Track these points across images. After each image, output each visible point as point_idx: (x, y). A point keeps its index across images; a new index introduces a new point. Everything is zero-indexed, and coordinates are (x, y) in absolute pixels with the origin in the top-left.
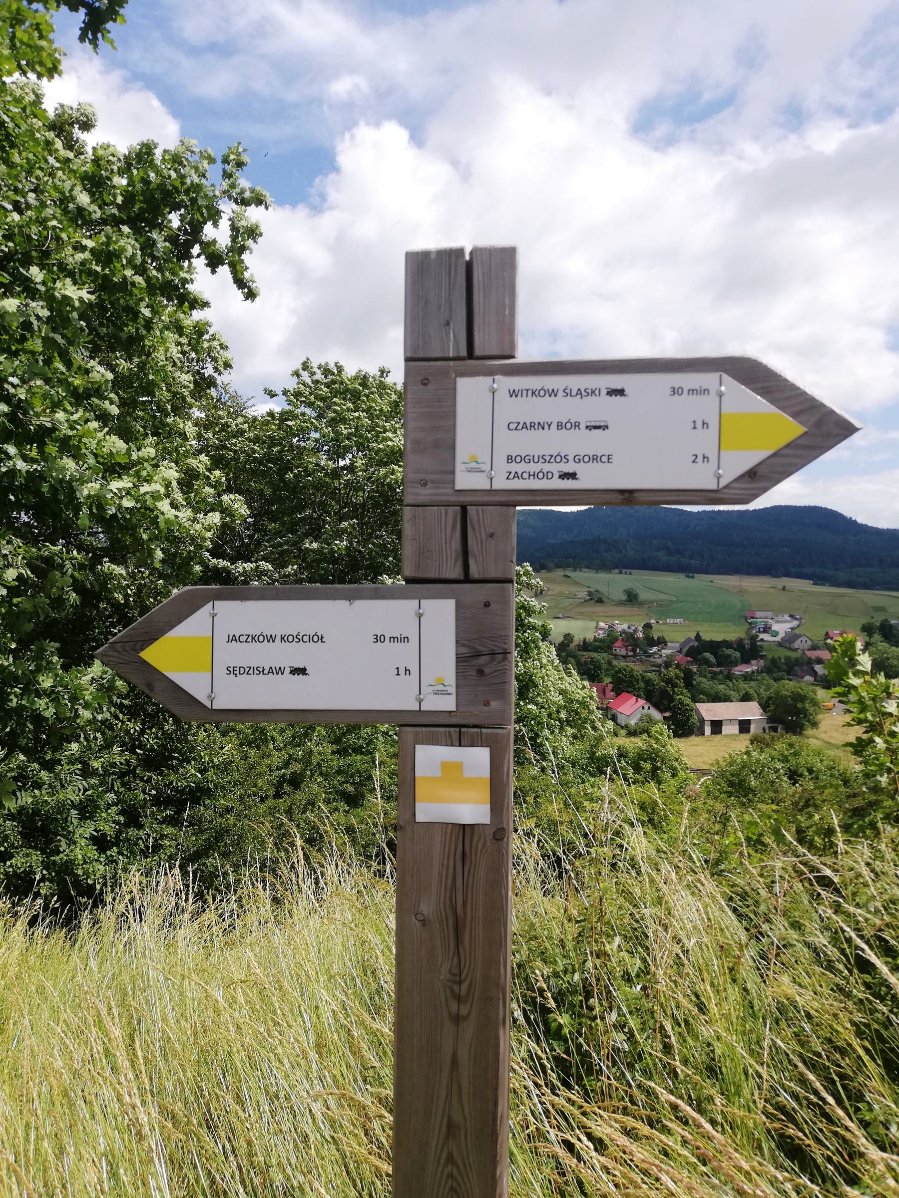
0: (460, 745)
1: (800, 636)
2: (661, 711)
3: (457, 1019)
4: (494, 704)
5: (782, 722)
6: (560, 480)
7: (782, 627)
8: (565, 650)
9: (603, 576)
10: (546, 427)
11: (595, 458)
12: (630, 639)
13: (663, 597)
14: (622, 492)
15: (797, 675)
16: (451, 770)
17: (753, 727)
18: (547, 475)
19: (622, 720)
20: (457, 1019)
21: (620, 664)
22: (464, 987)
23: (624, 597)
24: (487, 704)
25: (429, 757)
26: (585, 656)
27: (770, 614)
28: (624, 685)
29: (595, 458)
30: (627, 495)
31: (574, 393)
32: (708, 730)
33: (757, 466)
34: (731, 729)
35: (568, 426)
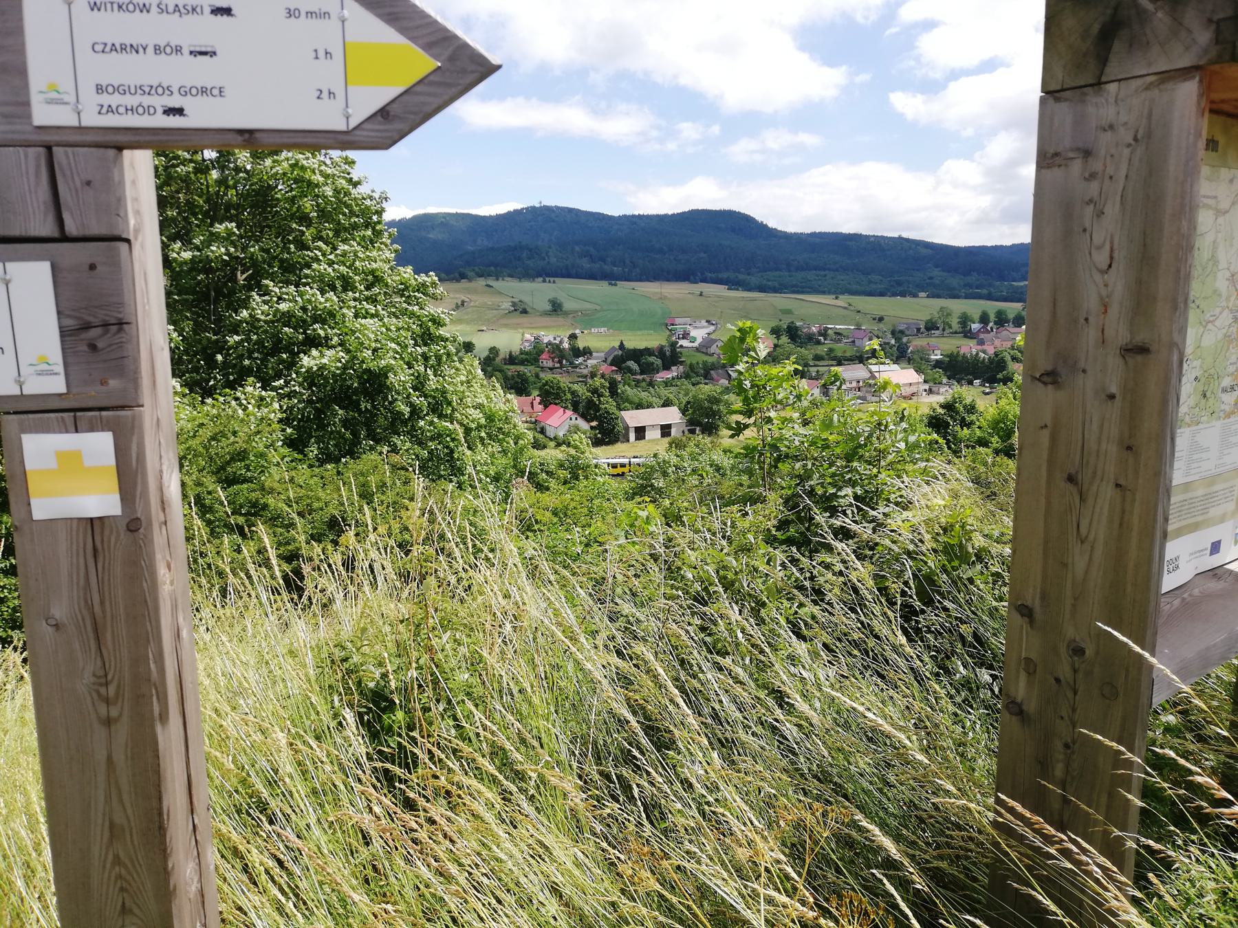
0: (77, 431)
1: (716, 341)
2: (588, 421)
3: (108, 722)
4: (113, 383)
5: (699, 424)
6: (165, 117)
7: (699, 334)
8: (490, 364)
9: (527, 285)
10: (141, 50)
11: (203, 91)
12: (556, 350)
13: (587, 306)
14: (241, 132)
15: (712, 379)
16: (70, 460)
17: (673, 431)
18: (149, 110)
19: (551, 432)
20: (108, 722)
21: (546, 376)
22: (112, 690)
23: (549, 307)
24: (103, 383)
25: (40, 449)
26: (512, 370)
27: (688, 320)
28: (551, 397)
29: (203, 91)
30: (247, 136)
31: (171, 9)
32: (632, 436)
33: (393, 101)
34: (653, 434)
35: (168, 50)
